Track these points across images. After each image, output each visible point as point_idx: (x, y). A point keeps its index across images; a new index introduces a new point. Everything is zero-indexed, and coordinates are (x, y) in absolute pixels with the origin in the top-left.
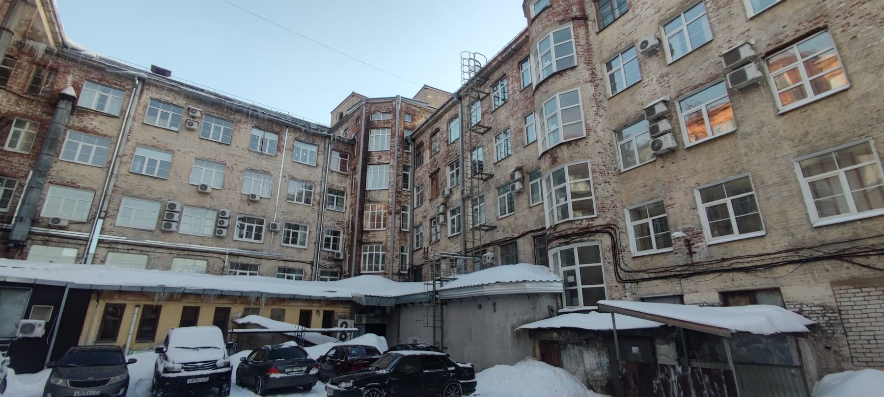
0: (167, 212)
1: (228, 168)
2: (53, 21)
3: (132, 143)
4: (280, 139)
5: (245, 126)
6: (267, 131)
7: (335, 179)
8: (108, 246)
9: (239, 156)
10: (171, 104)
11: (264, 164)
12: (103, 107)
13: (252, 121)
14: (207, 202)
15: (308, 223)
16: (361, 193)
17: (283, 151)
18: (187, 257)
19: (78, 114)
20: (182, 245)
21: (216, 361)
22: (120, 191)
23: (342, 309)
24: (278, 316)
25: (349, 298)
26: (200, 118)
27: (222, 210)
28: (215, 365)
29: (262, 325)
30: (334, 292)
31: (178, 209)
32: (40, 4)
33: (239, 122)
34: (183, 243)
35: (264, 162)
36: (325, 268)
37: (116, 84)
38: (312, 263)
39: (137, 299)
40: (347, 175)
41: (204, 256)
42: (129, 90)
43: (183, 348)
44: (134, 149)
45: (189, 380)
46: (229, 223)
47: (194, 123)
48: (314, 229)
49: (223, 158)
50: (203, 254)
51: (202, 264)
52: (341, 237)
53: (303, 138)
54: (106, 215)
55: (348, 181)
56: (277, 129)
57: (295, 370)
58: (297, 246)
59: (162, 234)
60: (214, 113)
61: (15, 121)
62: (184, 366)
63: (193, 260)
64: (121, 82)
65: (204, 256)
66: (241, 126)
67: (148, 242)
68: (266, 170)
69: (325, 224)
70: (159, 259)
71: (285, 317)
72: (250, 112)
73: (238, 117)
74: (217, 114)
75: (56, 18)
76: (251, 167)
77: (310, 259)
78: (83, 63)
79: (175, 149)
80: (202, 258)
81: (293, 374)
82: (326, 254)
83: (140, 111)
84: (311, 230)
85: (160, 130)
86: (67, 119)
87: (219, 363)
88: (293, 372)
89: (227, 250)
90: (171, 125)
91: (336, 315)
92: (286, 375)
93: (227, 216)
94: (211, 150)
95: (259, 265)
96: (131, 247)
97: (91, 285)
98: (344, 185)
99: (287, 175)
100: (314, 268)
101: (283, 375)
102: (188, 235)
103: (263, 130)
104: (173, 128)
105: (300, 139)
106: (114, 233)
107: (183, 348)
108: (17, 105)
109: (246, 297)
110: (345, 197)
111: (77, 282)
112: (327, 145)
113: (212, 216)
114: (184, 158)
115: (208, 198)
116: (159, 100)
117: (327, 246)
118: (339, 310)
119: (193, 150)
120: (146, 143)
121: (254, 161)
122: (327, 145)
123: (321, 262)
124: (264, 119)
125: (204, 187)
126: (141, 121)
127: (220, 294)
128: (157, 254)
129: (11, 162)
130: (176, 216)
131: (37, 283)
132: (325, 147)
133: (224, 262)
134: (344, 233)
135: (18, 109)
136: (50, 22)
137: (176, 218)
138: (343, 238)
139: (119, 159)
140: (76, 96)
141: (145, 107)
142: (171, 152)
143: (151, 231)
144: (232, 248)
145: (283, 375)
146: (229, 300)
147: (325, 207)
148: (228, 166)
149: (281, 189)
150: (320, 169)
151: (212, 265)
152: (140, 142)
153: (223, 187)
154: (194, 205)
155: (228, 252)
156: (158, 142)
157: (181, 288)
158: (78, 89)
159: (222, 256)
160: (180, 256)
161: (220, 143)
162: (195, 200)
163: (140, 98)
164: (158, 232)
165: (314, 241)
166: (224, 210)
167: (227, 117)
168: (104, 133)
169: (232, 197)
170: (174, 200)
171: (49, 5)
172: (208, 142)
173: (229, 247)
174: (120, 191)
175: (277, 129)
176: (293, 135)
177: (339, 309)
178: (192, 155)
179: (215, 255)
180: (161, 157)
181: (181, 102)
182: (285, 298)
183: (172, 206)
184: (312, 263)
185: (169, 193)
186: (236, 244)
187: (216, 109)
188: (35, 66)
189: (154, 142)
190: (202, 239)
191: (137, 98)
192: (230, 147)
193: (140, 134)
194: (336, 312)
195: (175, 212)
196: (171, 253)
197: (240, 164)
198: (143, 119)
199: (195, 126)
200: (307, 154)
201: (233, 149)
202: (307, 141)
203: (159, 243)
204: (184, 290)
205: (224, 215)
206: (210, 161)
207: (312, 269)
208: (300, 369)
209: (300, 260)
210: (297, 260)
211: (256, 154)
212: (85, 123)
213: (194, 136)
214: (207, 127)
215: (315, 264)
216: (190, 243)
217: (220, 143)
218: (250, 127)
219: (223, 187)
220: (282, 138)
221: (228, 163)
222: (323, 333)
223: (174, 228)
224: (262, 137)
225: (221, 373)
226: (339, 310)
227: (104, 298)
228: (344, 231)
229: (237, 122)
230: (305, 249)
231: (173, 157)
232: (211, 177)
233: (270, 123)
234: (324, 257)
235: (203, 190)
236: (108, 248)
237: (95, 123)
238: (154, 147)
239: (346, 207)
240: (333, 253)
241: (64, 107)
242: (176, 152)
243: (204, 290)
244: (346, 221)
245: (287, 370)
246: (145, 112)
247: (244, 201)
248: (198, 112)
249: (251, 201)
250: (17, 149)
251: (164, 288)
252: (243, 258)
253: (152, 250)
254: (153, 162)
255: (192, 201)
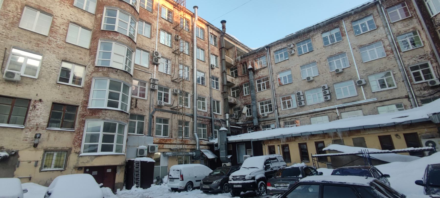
0: (297, 98)
1: (317, 62)
2: (244, 47)
3: (274, 74)
4: (341, 29)
5: (317, 36)
6: (330, 30)
7: (399, 27)
8: (283, 120)
9: (321, 53)
10: (281, 49)
11: (337, 49)
12: (262, 67)
13: (320, 31)
14: (314, 85)
15: (389, 69)
16: (426, 24)
17: (346, 35)
18: (316, 116)
19: (256, 73)
20: (311, 111)
21: (244, 176)
22: (278, 95)
23: (426, 130)
24: (360, 143)
25: (426, 118)
26: (294, 47)
27: (322, 86)
28: (244, 178)
29: (339, 150)
30: (406, 117)
31: (301, 94)
32: (236, 44)
33: (313, 36)
34: (311, 109)
35: (336, 48)
36: (424, 97)
37: (262, 55)
38: (407, 97)
39: (277, 142)
40: (412, 17)
41: (324, 113)
42: (266, 54)
43: (244, 168)
44: (276, 76)
45: (234, 185)
46: (329, 92)
47: (292, 51)
48: (396, 71)
49: (313, 59)
50: (323, 112)
51: (326, 118)
52: (431, 67)
53: (357, 18)
54: (277, 107)
55: (415, 21)
56: (336, 25)
57: (281, 185)
58: (388, 88)
59: (300, 109)
60: (299, 40)
61: (243, 85)
62: (233, 178)
63: (321, 117)
64: (263, 53)
65: (324, 113)
66: (315, 37)
67: (297, 113)
68: (339, 52)
69: (407, 63)
70: (304, 121)
71: (366, 142)
72: (315, 27)
73: (311, 34)
74: (301, 40)
75: (243, 45)
76: (330, 55)
77: (404, 94)
78: (250, 55)
79: (290, 67)
80: (323, 115)
81: (280, 188)
82: (419, 86)
83: (272, 59)
84: (394, 73)
85: (282, 62)
86: (253, 77)
87: (246, 178)
88: (280, 186)
89: (336, 106)
90: (285, 58)
91: (419, 136)
92: (276, 189)
93: (327, 88)
94: (305, 58)
95: (189, 122)
96: (291, 118)
97: (242, 140)
98: (412, 26)
99: (356, 47)
100: (411, 100)
101: (273, 188)
102: (312, 105)
103: (328, 31)
104: (286, 59)
105: (355, 19)
106: (283, 114)
107: (244, 168)
108: (242, 80)
109: (326, 134)
110: (418, 35)
111: (253, 138)
112: (379, 9)
113: (321, 91)
114: (296, 69)
115: (314, 83)
116: (277, 51)
117: (418, 78)
118: (421, 131)
119: (298, 63)
120: (279, 71)
121: (330, 51)
122: (379, 9)
123: (417, 93)
124: (324, 26)
125: (309, 78)
126: (274, 63)
127: (310, 134)
128: (302, 118)
129: (247, 99)
130: (302, 97)
131: (236, 141)
132: (378, 11)
133: (337, 113)
134: (432, 63)
135: (242, 81)
136: (243, 47)
137: (302, 99)
138: (433, 67)
139: (273, 83)
140: (252, 67)
141: (273, 57)
142: (289, 69)
143: (295, 108)
144: (338, 104)
145: (273, 188)
146: (320, 137)
147: (400, 51)
148: (317, 61)
149: (355, 57)
150: (382, 28)
151: (331, 117)
152: (277, 72)
153: (319, 73)
154: (309, 89)
155: (336, 107)
156: (283, 68)
157: (290, 134)
158: (253, 65)
159: (334, 111)
160: (313, 116)
161: (308, 53)
162: (308, 86)
163: (270, 55)
164: (298, 108)
165: (401, 80)
166: (324, 85)
167: (306, 38)
168: (265, 75)
169: (326, 76)
170: (299, 91)
171: (238, 43)
172: (303, 56)
173: (336, 104)
174: (278, 95)
175: (336, 25)
176: (349, 21)
177: (420, 130)
178: (298, 66)
179: (330, 111)
180: (286, 74)
181: (284, 45)
182: (360, 129)
183: (298, 94)
184: (407, 97)
185: (296, 88)
186: (340, 101)
187: (300, 38)
188: (241, 65)
189: (282, 69)
190: (320, 105)
191: (269, 55)
192: (314, 51)
193: (276, 69)
194: (418, 133)
195: (301, 96)
196: (308, 116)
197: (323, 57)
198: (275, 62)
199: (293, 52)
200: (365, 25)
201: (316, 52)
202: (361, 17)
203: (301, 113)
204: (292, 135)
205: (325, 88)
206: (308, 64)
207: (410, 101)
208: (285, 185)
209: (394, 97)
210: (391, 98)
211: (329, 47)
212: (259, 75)
213: (295, 57)
214: (300, 49)
215: (410, 96)
216: (315, 109)
217: (308, 53)
218: (319, 34)
219: (319, 73)
220: (342, 28)
221: (316, 60)
222: (412, 153)
223: (303, 104)
224: (330, 35)
225: (247, 183)
226: (421, 131)
227: (266, 144)
228: (431, 61)
229: (312, 37)
230: (395, 89)
231: (291, 71)
232: (310, 72)
233: (331, 25)
234: (419, 89)
235: (309, 80)
236: (283, 121)
237: (261, 73)
238: (283, 71)
239: (423, 42)
240: (426, 82)
241: (251, 73)
242: (291, 68)
243: (301, 133)
244: (429, 53)
245: (275, 185)
246: (274, 59)
247: (334, 75)
248: (291, 45)
249: (338, 74)
250: (247, 94)
251: (283, 136)
252: (348, 108)
253: (299, 117)
254: (285, 78)
255: (307, 88)
